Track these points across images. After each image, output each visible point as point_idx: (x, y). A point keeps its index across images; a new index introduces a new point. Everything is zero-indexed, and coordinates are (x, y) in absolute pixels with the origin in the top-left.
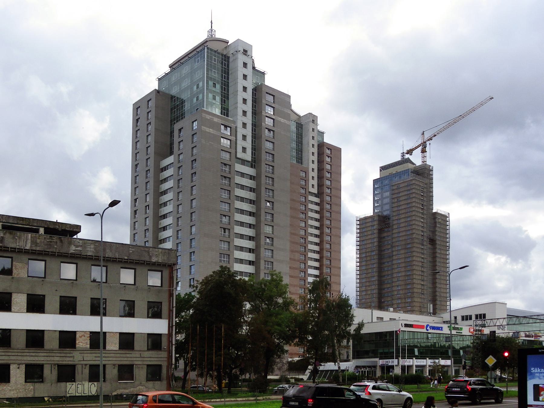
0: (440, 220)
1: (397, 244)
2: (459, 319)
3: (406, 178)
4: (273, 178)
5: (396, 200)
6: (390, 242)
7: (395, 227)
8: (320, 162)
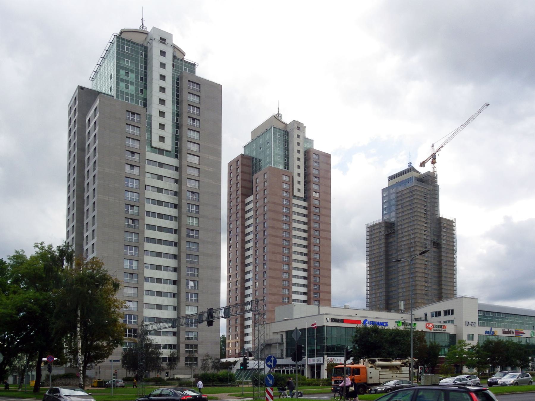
0: (445, 225)
1: (401, 248)
2: (429, 315)
3: (409, 185)
5: (400, 207)
7: (400, 232)
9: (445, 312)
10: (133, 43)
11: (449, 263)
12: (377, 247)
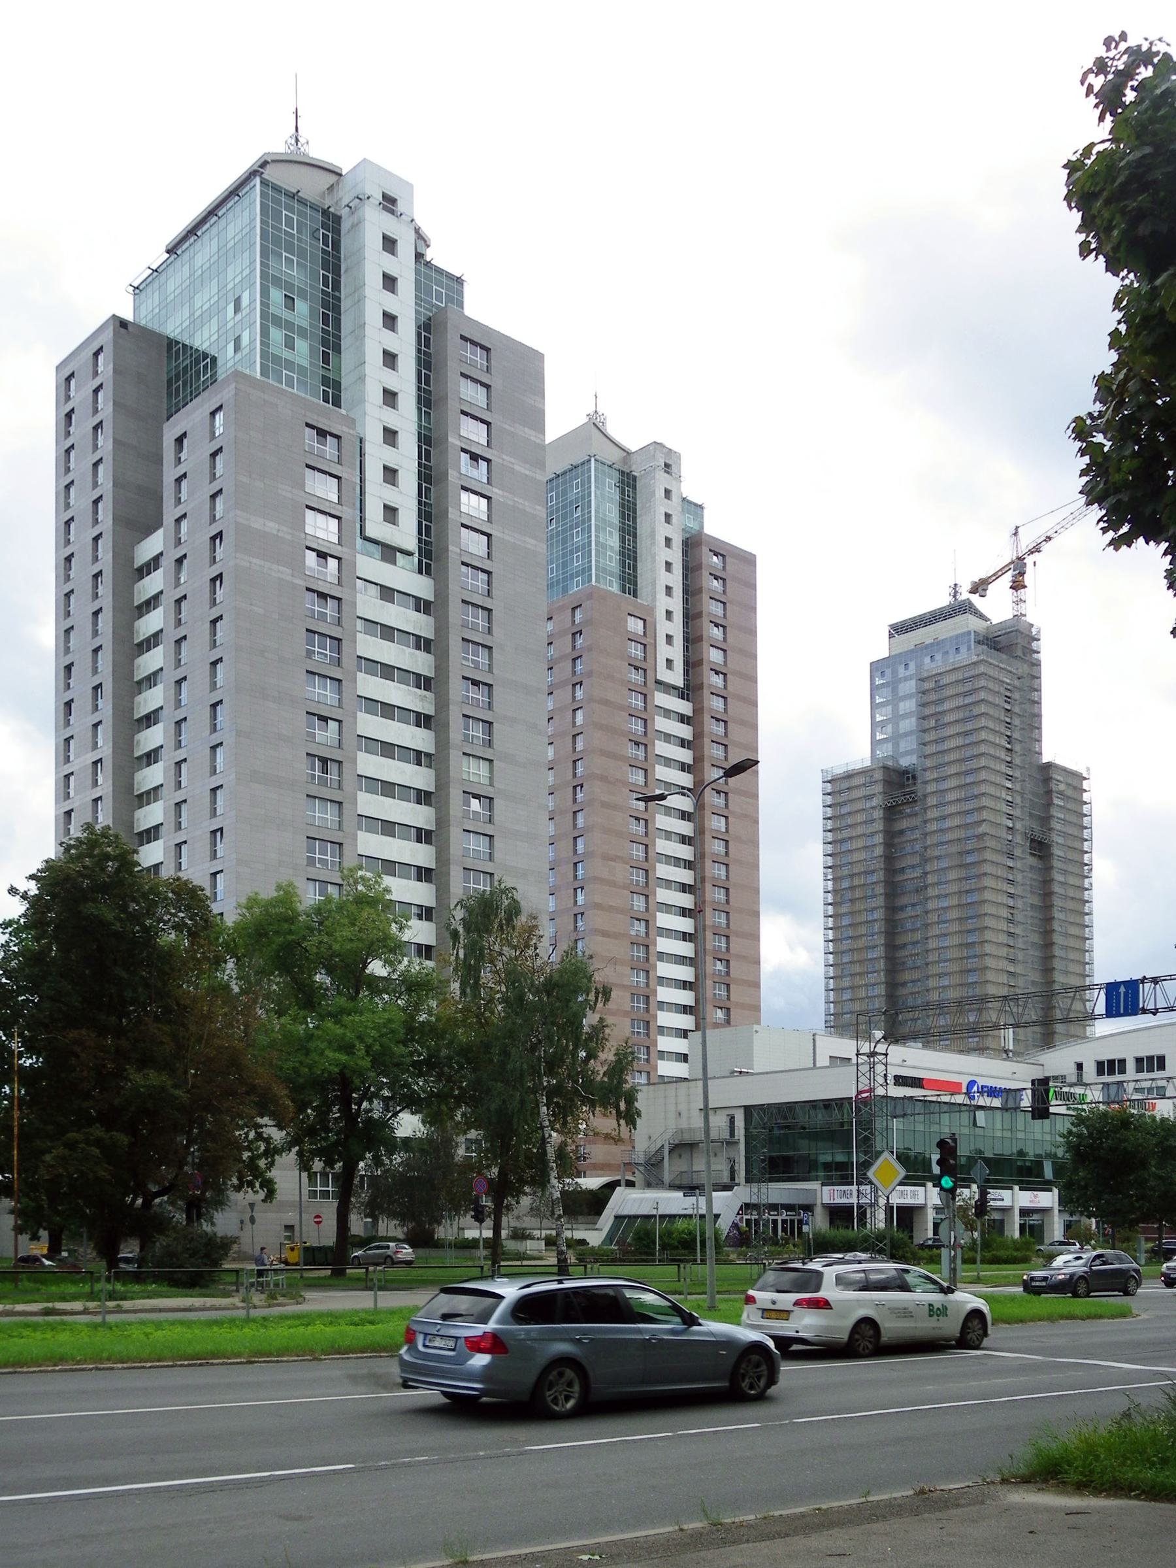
0: (1062, 787)
3: (966, 656)
4: (489, 610)
6: (918, 847)
7: (932, 801)
8: (691, 592)
9: (1139, 1061)
10: (303, 202)
11: (1071, 905)
12: (860, 843)
